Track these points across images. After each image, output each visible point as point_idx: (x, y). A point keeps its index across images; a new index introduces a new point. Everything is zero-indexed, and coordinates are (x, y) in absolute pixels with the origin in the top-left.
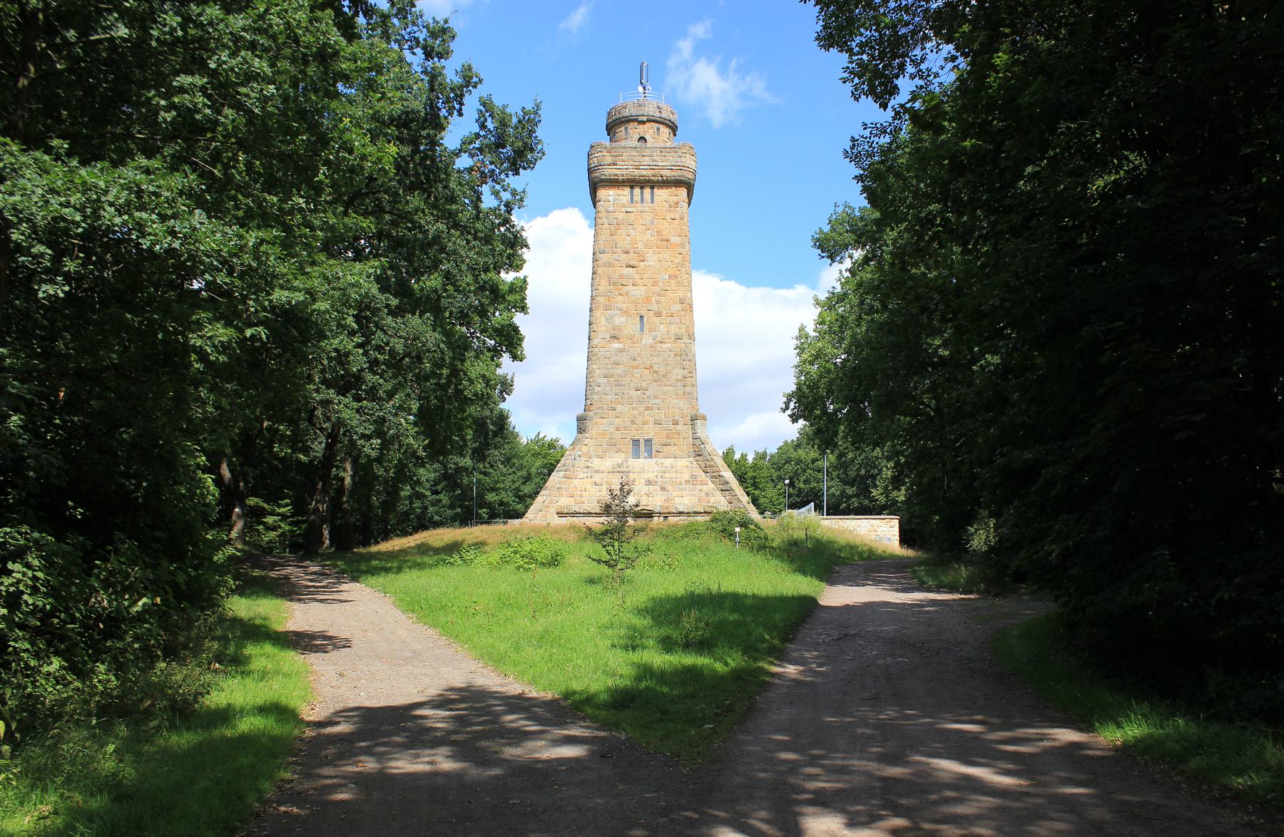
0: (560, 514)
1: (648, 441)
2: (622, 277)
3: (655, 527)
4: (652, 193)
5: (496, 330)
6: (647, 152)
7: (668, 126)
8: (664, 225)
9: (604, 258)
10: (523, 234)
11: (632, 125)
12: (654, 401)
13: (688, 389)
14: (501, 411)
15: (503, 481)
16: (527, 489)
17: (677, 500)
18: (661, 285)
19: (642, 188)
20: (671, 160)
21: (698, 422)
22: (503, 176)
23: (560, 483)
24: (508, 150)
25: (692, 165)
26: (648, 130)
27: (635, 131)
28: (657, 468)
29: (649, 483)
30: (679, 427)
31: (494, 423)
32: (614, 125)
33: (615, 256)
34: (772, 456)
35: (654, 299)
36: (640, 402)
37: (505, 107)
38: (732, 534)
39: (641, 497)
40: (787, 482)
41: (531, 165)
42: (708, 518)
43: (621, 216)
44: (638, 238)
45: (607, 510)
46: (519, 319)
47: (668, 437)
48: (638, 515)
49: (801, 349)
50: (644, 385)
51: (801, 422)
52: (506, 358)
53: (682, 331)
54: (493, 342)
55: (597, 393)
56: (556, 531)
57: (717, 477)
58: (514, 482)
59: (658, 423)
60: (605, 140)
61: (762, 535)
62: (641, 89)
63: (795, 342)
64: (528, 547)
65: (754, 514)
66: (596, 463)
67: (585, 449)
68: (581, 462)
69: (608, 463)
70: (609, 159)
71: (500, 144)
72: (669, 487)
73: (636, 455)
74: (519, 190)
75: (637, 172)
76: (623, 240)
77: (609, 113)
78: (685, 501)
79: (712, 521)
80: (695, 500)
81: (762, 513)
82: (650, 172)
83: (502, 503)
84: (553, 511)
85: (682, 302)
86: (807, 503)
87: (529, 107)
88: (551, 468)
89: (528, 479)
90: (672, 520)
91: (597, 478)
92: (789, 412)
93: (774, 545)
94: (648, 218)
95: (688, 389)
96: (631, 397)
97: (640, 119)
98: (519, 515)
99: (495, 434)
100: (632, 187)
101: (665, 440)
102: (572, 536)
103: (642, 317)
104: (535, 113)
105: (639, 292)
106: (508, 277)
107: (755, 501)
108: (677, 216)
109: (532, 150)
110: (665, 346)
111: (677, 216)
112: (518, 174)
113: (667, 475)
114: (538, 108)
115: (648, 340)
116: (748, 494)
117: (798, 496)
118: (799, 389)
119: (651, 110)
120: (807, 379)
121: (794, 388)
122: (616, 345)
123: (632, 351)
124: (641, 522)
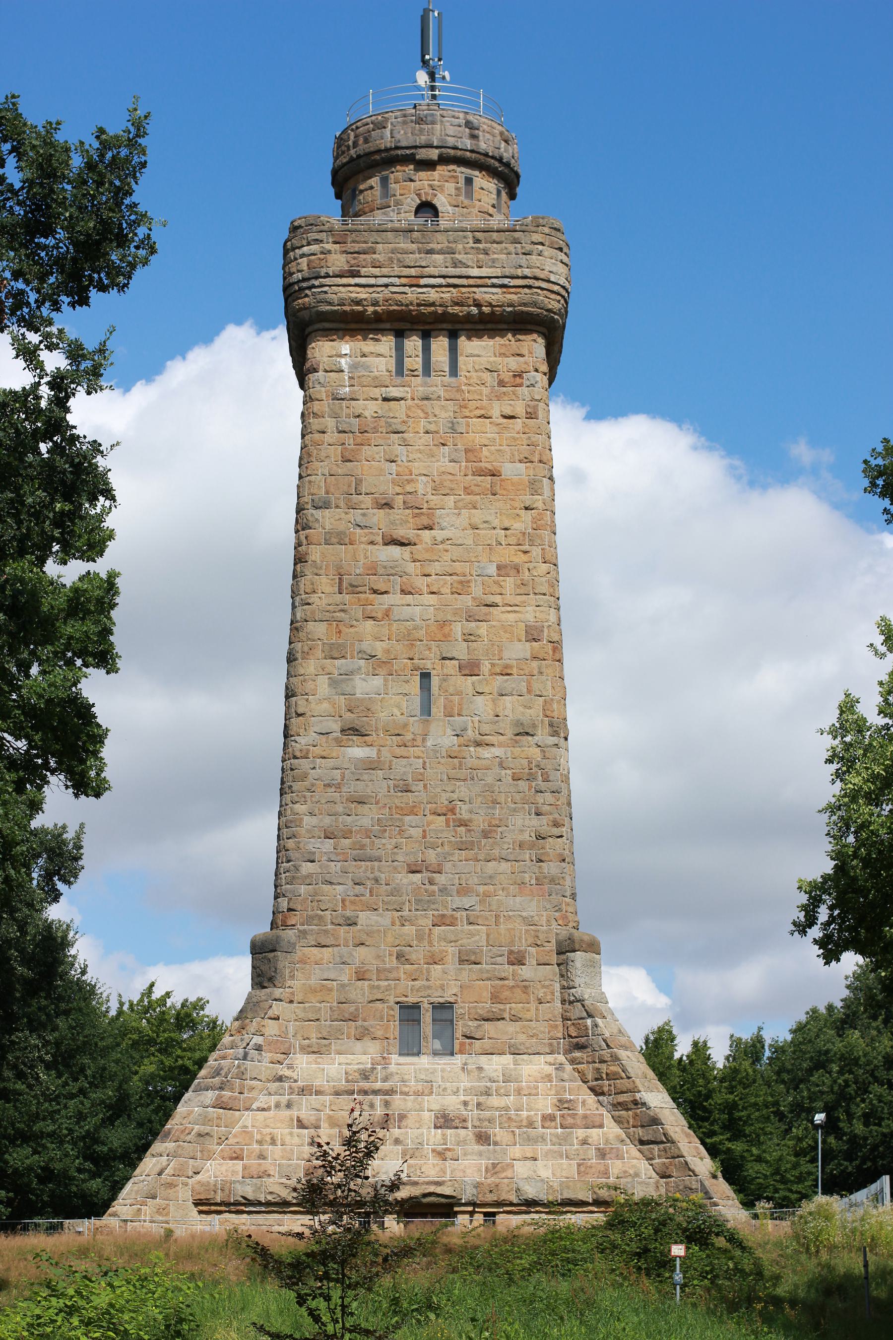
0: (205, 1205)
1: (444, 1009)
2: (372, 570)
3: (456, 1241)
4: (453, 351)
5: (30, 711)
6: (439, 242)
7: (493, 172)
8: (481, 433)
9: (326, 520)
10: (100, 461)
11: (400, 172)
12: (458, 901)
13: (551, 868)
14: (49, 926)
15: (52, 1114)
16: (117, 1137)
17: (522, 1169)
18: (477, 590)
19: (426, 336)
20: (504, 259)
21: (579, 957)
22: (45, 311)
23: (205, 1120)
24: (58, 242)
25: (559, 274)
26: (442, 186)
27: (408, 187)
28: (465, 1083)
29: (444, 1121)
30: (525, 972)
31: (27, 961)
32: (357, 169)
33: (356, 515)
34: (779, 1050)
35: (458, 629)
36: (422, 904)
37: (52, 127)
38: (667, 1263)
39: (408, 1160)
40: (819, 1118)
41: (118, 279)
42: (599, 1218)
43: (370, 409)
44: (417, 467)
45: (312, 1197)
46: (94, 686)
47: (495, 998)
48: (411, 1209)
49: (843, 762)
50: (432, 856)
51: (851, 961)
52: (56, 793)
53: (535, 712)
54: (22, 744)
55: (308, 880)
56: (191, 1252)
57: (628, 1108)
58: (81, 1117)
59: (467, 959)
60: (330, 210)
61: (747, 1265)
62: (422, 78)
63: (828, 742)
64: (102, 1298)
65: (729, 1208)
66: (303, 1066)
67: (271, 1028)
68: (262, 1065)
69: (334, 1068)
70: (338, 261)
71: (39, 221)
72: (498, 1133)
73: (410, 1048)
74: (90, 345)
75: (412, 295)
76: (376, 473)
77: (340, 141)
78: (542, 1170)
79: (610, 1225)
80: (569, 1168)
81: (748, 1204)
82: (447, 295)
83: (47, 1175)
84: (185, 1195)
85: (532, 636)
86: (873, 1177)
87: (117, 127)
88: (184, 1078)
89: (118, 1109)
90: (507, 1222)
91: (305, 1108)
92: (816, 932)
93: (781, 1291)
94: (444, 412)
95: (551, 868)
96: (395, 892)
97: (422, 154)
98: (96, 1207)
99: (32, 988)
100: (400, 334)
101: (486, 1007)
102: (233, 1268)
103: (426, 676)
104: (132, 143)
105: (419, 610)
106: (65, 572)
107: (732, 1171)
108: (520, 409)
109: (122, 240)
110: (487, 753)
111: (520, 409)
112: (84, 301)
113: (494, 1101)
114: (139, 127)
115: (442, 737)
116: (713, 1151)
117: (849, 1156)
118: (840, 870)
119: (448, 131)
120: (860, 843)
121: (828, 866)
122: (358, 752)
123: (401, 768)
124: (421, 1227)
